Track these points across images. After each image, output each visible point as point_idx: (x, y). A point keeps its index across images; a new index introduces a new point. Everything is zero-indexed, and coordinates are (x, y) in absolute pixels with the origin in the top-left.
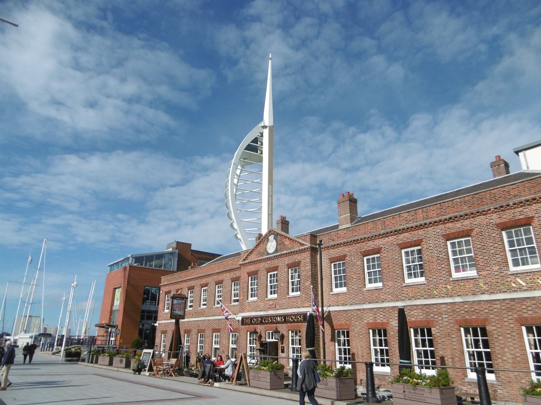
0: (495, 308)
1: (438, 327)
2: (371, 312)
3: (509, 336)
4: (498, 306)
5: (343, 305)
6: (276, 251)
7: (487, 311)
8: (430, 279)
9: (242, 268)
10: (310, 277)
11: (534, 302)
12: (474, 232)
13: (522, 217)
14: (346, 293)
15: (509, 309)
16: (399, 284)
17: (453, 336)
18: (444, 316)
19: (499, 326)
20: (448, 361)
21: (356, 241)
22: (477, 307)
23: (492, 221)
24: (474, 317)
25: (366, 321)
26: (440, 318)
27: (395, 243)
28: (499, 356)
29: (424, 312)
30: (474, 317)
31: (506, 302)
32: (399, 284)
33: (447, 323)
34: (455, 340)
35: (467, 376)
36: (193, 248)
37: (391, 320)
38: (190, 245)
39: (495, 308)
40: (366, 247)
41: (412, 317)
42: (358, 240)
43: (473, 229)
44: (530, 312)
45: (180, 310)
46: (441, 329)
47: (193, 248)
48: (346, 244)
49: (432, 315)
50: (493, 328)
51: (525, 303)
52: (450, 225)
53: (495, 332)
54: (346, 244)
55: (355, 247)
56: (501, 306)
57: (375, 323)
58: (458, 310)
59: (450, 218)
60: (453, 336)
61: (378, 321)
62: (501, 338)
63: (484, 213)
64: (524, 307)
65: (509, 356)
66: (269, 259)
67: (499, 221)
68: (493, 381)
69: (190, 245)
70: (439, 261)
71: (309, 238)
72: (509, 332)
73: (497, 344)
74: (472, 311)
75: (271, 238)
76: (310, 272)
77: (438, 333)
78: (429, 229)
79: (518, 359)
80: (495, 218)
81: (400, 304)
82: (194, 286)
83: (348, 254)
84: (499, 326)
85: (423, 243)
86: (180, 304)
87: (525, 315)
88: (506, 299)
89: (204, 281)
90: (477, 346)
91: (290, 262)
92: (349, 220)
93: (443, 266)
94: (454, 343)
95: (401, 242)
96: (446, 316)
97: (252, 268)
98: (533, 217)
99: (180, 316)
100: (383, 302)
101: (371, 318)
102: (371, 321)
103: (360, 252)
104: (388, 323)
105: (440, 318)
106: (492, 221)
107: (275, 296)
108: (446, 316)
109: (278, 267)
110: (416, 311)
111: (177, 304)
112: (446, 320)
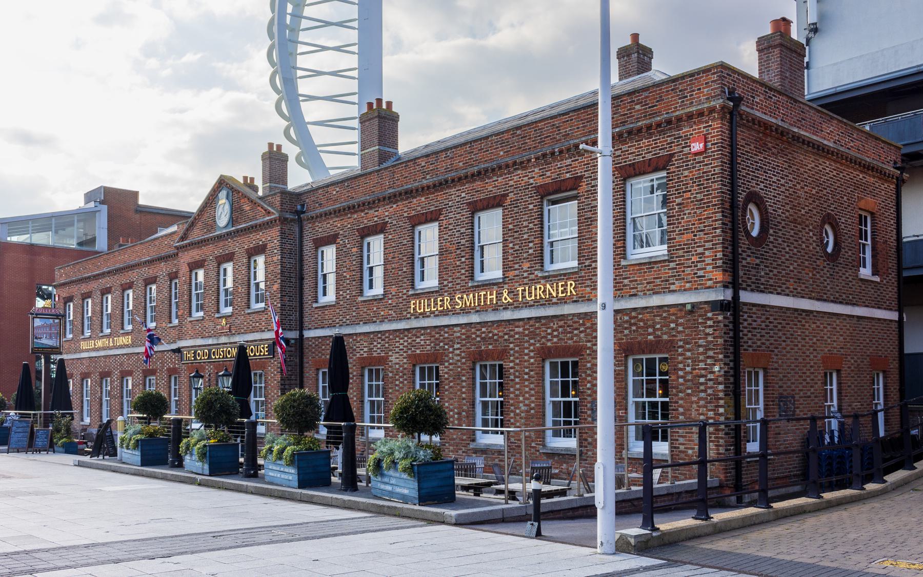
0: (517, 333)
1: (446, 364)
2: (366, 339)
3: (526, 377)
4: (521, 330)
5: (331, 326)
6: (233, 221)
7: (506, 337)
8: (445, 283)
9: (180, 255)
10: (279, 276)
11: (561, 323)
12: (508, 202)
13: (568, 175)
14: (334, 306)
15: (533, 335)
16: (405, 291)
17: (464, 378)
18: (456, 346)
19: (517, 361)
20: (453, 417)
21: (352, 209)
22: (496, 331)
23: (531, 181)
24: (490, 347)
25: (358, 355)
26: (451, 350)
27: (406, 215)
28: (512, 408)
29: (433, 339)
30: (490, 347)
31: (532, 322)
32: (405, 291)
33: (459, 358)
34: (464, 384)
35: (474, 440)
36: (142, 201)
37: (390, 353)
38: (135, 194)
39: (517, 333)
40: (366, 221)
41: (356, 354)
42: (354, 207)
43: (507, 195)
44: (555, 340)
45: (51, 338)
46: (451, 367)
47: (142, 201)
48: (338, 213)
49: (441, 344)
50: (512, 365)
51: (552, 324)
52: (478, 184)
53: (512, 371)
54: (338, 213)
55: (350, 221)
56: (524, 330)
57: (370, 358)
58: (474, 336)
59: (479, 173)
60: (464, 378)
61: (375, 354)
62: (517, 380)
63: (522, 165)
64: (549, 331)
65: (523, 408)
66: (220, 237)
67: (540, 181)
68: (501, 446)
69: (135, 194)
70: (458, 252)
71: (278, 199)
72: (527, 370)
73: (512, 390)
74: (490, 338)
75: (223, 194)
76: (279, 267)
77: (446, 373)
78: (453, 191)
79: (532, 411)
80: (536, 176)
81: (240, 339)
82: (111, 287)
83: (341, 232)
84: (517, 361)
85: (442, 217)
86: (51, 326)
87: (549, 344)
88: (540, 318)
89: (84, 288)
90: (651, 393)
91: (252, 246)
92: (377, 159)
93: (463, 259)
94: (464, 390)
95: (413, 213)
96: (459, 346)
98: (581, 177)
99: (52, 348)
100: (382, 321)
101: (366, 349)
102: (365, 355)
103: (358, 230)
104: (387, 358)
105: (451, 350)
106: (531, 181)
107: (201, 314)
108: (459, 346)
109: (233, 253)
110: (422, 337)
111: (42, 327)
112: (458, 352)
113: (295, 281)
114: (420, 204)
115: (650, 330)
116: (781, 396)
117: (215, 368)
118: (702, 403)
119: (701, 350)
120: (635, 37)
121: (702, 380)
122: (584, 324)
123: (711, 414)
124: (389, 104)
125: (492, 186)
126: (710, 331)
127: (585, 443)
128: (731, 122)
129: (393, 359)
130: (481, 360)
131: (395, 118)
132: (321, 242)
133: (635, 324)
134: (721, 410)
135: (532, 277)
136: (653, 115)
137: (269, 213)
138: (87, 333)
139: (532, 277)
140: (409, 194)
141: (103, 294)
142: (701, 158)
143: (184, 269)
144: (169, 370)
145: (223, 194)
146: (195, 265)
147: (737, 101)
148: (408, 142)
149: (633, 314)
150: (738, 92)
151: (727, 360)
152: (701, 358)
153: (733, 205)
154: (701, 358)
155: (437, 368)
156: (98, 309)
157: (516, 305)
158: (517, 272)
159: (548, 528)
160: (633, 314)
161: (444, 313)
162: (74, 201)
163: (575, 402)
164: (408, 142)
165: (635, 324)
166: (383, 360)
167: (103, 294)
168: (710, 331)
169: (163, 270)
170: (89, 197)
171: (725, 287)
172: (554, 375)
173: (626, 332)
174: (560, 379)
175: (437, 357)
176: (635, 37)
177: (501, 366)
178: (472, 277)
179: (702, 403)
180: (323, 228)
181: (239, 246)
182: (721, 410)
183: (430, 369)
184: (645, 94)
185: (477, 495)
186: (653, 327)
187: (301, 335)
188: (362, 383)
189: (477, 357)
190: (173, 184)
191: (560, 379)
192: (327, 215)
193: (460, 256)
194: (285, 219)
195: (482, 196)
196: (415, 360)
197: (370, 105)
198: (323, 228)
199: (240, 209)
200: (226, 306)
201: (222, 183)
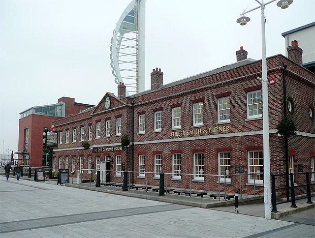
5: (143, 141)
48: (146, 104)
75: (107, 98)
80: (215, 92)
97: (97, 118)
98: (231, 92)
113: (131, 126)
114: (175, 101)
115: (256, 142)
116: (299, 165)
117: (104, 154)
118: (275, 167)
119: (274, 149)
120: (242, 48)
121: (275, 159)
122: (232, 140)
123: (278, 171)
124: (160, 69)
125: (199, 96)
126: (278, 143)
127: (233, 180)
128: (283, 74)
129: (165, 152)
130: (196, 152)
131: (162, 74)
132: (139, 114)
133: (250, 140)
134: (282, 170)
135: (214, 125)
136: (256, 72)
137: (124, 104)
138: (61, 143)
139: (214, 125)
140: (171, 98)
141: (66, 131)
142: (273, 85)
143: (94, 122)
144: (88, 155)
145: (107, 98)
146: (97, 121)
147: (286, 67)
148: (167, 81)
149: (250, 137)
150: (285, 64)
151: (283, 153)
152: (274, 152)
153: (285, 102)
154: (274, 152)
155: (180, 155)
156: (65, 135)
157: (208, 134)
158: (208, 123)
159: (240, 208)
160: (250, 137)
161: (183, 136)
162: (55, 102)
163: (229, 166)
164: (167, 81)
165: (250, 140)
166: (161, 152)
167: (66, 131)
168: (278, 143)
169: (86, 123)
170: (59, 100)
171: (276, 129)
172: (196, 158)
173: (247, 143)
174: (258, 158)
175: (180, 151)
176: (242, 48)
177: (203, 154)
178: (192, 125)
179: (275, 167)
180: (140, 109)
181: (112, 115)
182: (282, 170)
183: (200, 155)
184: (254, 65)
185: (179, 194)
186: (257, 141)
187: (133, 144)
188: (217, 158)
189: (194, 151)
190: (90, 95)
191: (258, 158)
192: (140, 105)
193: (187, 120)
194: (122, 106)
195: (196, 98)
196: (173, 152)
197: (154, 70)
198: (140, 109)
199: (113, 102)
200: (141, 130)
201: (107, 95)
